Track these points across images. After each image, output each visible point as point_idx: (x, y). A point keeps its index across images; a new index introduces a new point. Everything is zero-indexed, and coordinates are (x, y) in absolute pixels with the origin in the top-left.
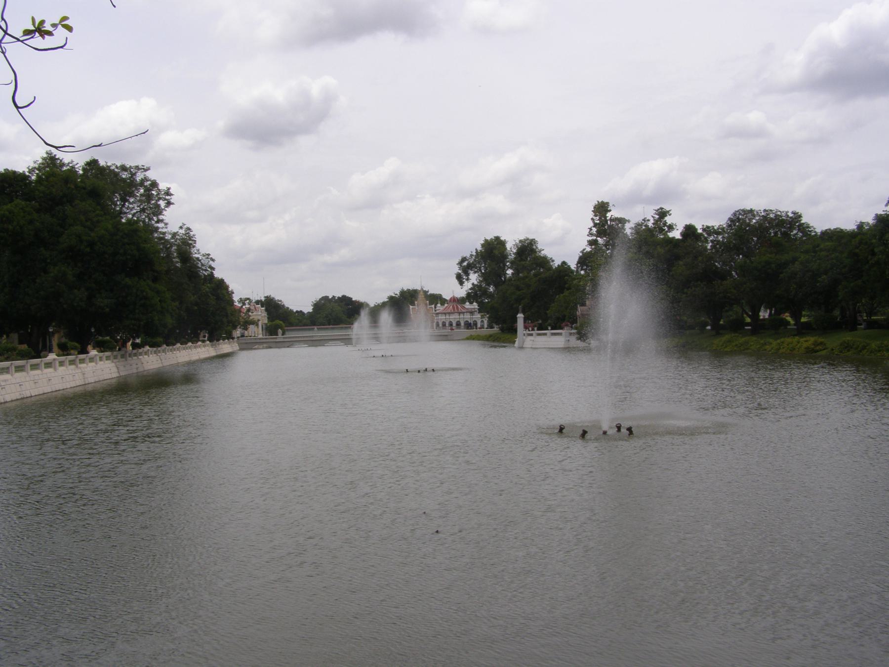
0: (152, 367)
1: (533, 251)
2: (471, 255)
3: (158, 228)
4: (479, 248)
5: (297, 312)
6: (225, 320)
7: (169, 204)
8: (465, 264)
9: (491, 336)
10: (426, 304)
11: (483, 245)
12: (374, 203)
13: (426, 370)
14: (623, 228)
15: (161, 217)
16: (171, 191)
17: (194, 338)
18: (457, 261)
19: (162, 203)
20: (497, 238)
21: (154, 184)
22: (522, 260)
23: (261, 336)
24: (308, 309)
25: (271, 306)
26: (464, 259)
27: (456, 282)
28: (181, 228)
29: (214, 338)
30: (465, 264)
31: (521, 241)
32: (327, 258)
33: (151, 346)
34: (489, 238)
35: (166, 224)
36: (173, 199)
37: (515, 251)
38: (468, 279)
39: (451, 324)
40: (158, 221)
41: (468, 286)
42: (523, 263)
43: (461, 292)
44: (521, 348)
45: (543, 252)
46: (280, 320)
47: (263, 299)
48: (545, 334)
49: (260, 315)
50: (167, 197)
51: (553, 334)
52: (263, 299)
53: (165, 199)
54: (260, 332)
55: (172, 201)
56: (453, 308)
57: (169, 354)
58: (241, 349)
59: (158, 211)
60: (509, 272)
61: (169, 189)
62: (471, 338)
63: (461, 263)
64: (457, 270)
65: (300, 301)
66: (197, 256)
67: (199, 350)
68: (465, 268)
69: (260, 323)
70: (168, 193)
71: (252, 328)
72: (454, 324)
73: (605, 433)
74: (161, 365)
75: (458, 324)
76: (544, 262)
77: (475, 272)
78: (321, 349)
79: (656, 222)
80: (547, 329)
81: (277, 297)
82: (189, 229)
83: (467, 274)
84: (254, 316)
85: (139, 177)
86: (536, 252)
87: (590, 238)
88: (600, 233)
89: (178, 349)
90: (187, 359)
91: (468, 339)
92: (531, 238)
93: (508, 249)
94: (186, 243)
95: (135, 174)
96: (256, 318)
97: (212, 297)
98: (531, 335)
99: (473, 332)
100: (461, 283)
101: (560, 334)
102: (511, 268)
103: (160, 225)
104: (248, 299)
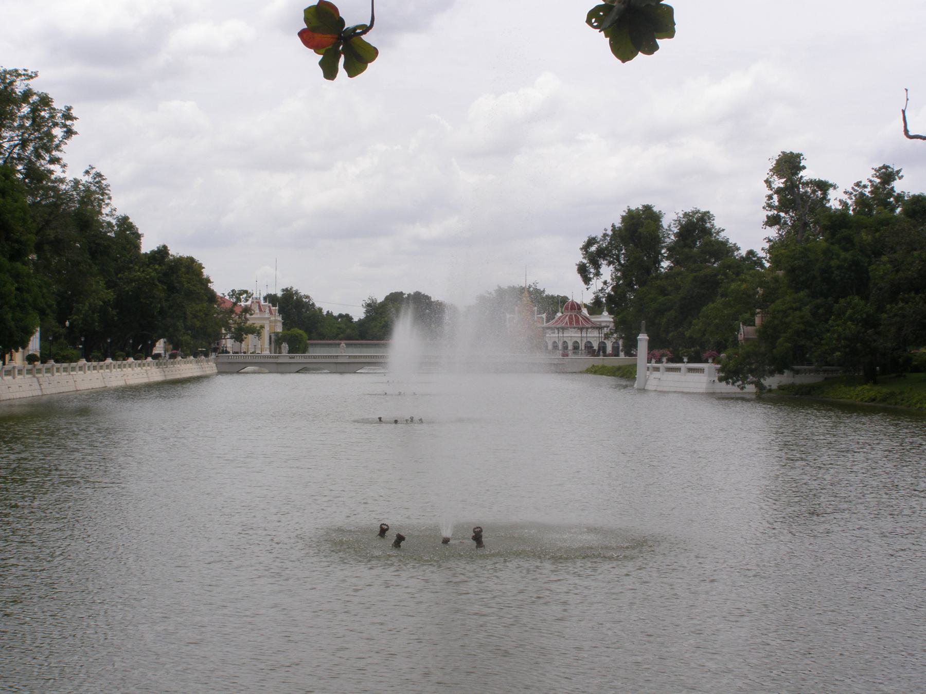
0: (18, 395)
1: (707, 232)
2: (605, 235)
3: (51, 172)
4: (618, 224)
5: (341, 316)
6: (180, 324)
7: (69, 133)
8: (593, 249)
9: (619, 368)
10: (532, 312)
11: (624, 219)
12: (505, 146)
13: (412, 419)
14: (825, 198)
15: (55, 153)
16: (74, 113)
17: (139, 349)
18: (581, 244)
19: (58, 132)
20: (648, 208)
21: (45, 101)
22: (685, 246)
23: (267, 353)
24: (358, 314)
25: (293, 308)
26: (591, 242)
27: (578, 277)
28: (87, 172)
29: (179, 349)
30: (593, 249)
31: (686, 215)
32: (423, 231)
33: (57, 361)
34: (633, 208)
35: (64, 166)
36: (76, 126)
37: (676, 230)
38: (598, 274)
39: (565, 347)
40: (55, 160)
41: (596, 284)
42: (686, 250)
43: (583, 294)
44: (643, 390)
45: (722, 234)
46: (303, 329)
47: (280, 294)
48: (679, 370)
49: (271, 322)
50: (68, 123)
51: (690, 370)
52: (280, 294)
53: (65, 126)
54: (267, 345)
55: (74, 128)
56: (571, 319)
57: (116, 372)
58: (220, 373)
59: (47, 144)
60: (665, 264)
61: (69, 109)
62: (595, 371)
63: (586, 248)
64: (580, 257)
65: (340, 295)
66: (108, 219)
67: (128, 371)
68: (594, 256)
69: (266, 334)
70: (68, 116)
71: (250, 339)
72: (570, 347)
73: (446, 541)
74: (40, 394)
75: (576, 347)
76: (723, 250)
77: (609, 263)
78: (349, 378)
79: (876, 189)
80: (681, 361)
81: (303, 289)
82: (99, 175)
83: (597, 266)
84: (254, 319)
85: (20, 87)
86: (710, 234)
87: (770, 213)
88: (784, 205)
89: (108, 367)
90: (120, 383)
91: (297, 372)
92: (703, 210)
93: (665, 225)
94: (92, 194)
95: (11, 83)
96: (258, 324)
97: (160, 286)
98: (657, 369)
99: (599, 361)
100: (587, 280)
101: (701, 371)
102: (668, 258)
103: (55, 167)
104: (246, 292)
